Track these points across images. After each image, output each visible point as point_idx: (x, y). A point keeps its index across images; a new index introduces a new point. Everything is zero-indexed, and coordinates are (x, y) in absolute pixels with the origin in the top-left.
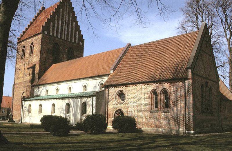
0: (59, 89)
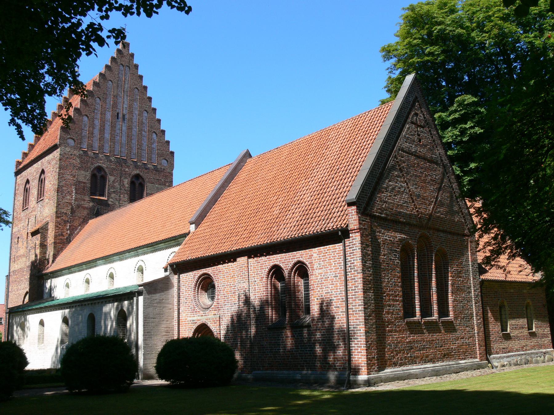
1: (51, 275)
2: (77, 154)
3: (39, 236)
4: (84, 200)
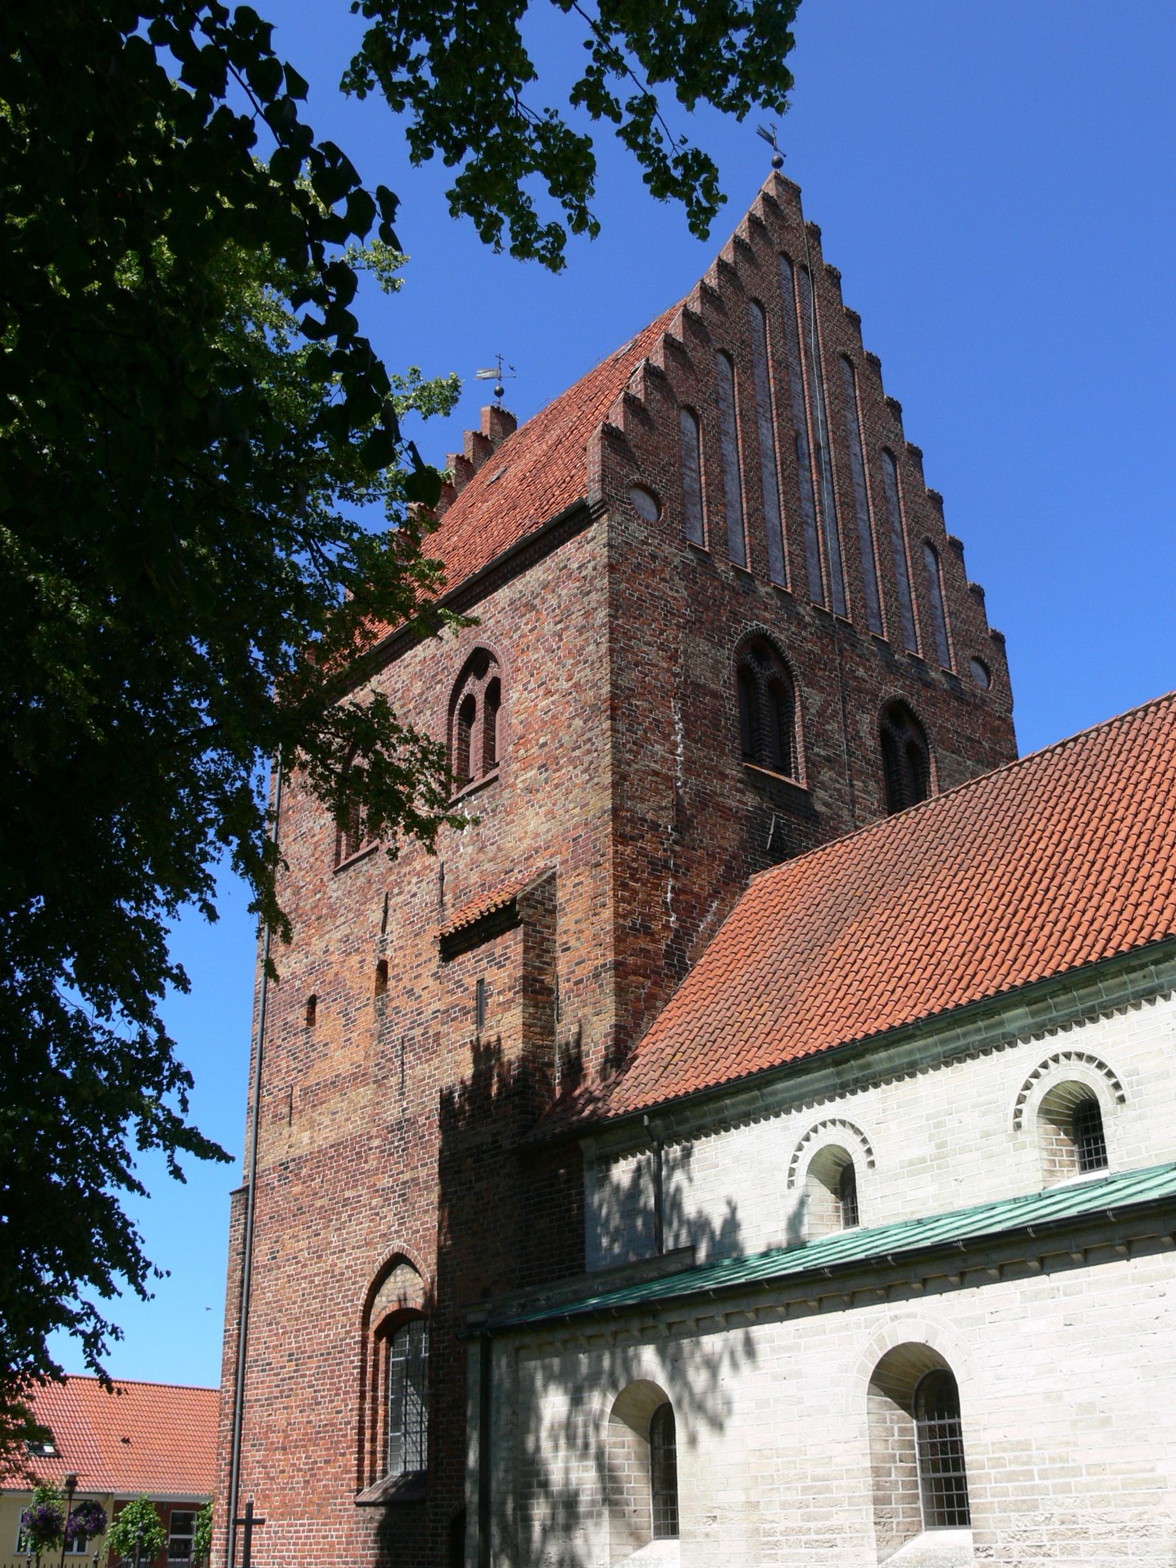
0: (1106, 1101)
1: (658, 1122)
2: (676, 561)
3: (511, 943)
4: (723, 776)
